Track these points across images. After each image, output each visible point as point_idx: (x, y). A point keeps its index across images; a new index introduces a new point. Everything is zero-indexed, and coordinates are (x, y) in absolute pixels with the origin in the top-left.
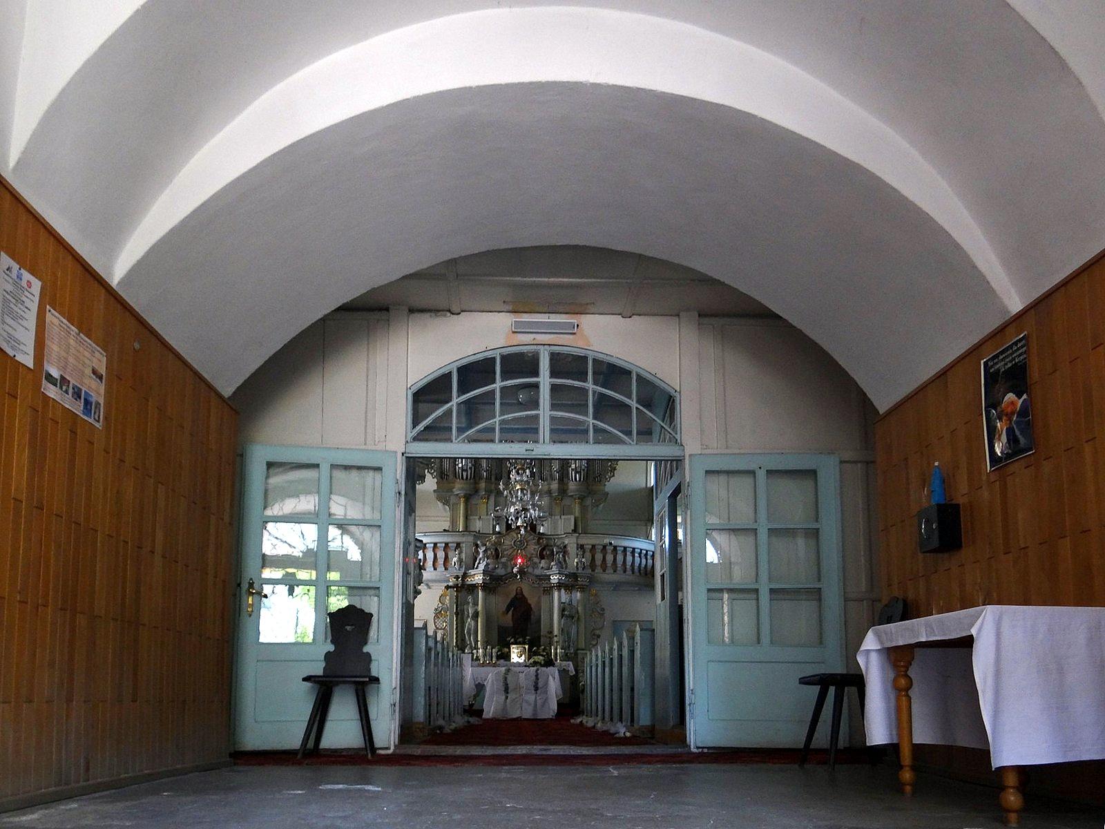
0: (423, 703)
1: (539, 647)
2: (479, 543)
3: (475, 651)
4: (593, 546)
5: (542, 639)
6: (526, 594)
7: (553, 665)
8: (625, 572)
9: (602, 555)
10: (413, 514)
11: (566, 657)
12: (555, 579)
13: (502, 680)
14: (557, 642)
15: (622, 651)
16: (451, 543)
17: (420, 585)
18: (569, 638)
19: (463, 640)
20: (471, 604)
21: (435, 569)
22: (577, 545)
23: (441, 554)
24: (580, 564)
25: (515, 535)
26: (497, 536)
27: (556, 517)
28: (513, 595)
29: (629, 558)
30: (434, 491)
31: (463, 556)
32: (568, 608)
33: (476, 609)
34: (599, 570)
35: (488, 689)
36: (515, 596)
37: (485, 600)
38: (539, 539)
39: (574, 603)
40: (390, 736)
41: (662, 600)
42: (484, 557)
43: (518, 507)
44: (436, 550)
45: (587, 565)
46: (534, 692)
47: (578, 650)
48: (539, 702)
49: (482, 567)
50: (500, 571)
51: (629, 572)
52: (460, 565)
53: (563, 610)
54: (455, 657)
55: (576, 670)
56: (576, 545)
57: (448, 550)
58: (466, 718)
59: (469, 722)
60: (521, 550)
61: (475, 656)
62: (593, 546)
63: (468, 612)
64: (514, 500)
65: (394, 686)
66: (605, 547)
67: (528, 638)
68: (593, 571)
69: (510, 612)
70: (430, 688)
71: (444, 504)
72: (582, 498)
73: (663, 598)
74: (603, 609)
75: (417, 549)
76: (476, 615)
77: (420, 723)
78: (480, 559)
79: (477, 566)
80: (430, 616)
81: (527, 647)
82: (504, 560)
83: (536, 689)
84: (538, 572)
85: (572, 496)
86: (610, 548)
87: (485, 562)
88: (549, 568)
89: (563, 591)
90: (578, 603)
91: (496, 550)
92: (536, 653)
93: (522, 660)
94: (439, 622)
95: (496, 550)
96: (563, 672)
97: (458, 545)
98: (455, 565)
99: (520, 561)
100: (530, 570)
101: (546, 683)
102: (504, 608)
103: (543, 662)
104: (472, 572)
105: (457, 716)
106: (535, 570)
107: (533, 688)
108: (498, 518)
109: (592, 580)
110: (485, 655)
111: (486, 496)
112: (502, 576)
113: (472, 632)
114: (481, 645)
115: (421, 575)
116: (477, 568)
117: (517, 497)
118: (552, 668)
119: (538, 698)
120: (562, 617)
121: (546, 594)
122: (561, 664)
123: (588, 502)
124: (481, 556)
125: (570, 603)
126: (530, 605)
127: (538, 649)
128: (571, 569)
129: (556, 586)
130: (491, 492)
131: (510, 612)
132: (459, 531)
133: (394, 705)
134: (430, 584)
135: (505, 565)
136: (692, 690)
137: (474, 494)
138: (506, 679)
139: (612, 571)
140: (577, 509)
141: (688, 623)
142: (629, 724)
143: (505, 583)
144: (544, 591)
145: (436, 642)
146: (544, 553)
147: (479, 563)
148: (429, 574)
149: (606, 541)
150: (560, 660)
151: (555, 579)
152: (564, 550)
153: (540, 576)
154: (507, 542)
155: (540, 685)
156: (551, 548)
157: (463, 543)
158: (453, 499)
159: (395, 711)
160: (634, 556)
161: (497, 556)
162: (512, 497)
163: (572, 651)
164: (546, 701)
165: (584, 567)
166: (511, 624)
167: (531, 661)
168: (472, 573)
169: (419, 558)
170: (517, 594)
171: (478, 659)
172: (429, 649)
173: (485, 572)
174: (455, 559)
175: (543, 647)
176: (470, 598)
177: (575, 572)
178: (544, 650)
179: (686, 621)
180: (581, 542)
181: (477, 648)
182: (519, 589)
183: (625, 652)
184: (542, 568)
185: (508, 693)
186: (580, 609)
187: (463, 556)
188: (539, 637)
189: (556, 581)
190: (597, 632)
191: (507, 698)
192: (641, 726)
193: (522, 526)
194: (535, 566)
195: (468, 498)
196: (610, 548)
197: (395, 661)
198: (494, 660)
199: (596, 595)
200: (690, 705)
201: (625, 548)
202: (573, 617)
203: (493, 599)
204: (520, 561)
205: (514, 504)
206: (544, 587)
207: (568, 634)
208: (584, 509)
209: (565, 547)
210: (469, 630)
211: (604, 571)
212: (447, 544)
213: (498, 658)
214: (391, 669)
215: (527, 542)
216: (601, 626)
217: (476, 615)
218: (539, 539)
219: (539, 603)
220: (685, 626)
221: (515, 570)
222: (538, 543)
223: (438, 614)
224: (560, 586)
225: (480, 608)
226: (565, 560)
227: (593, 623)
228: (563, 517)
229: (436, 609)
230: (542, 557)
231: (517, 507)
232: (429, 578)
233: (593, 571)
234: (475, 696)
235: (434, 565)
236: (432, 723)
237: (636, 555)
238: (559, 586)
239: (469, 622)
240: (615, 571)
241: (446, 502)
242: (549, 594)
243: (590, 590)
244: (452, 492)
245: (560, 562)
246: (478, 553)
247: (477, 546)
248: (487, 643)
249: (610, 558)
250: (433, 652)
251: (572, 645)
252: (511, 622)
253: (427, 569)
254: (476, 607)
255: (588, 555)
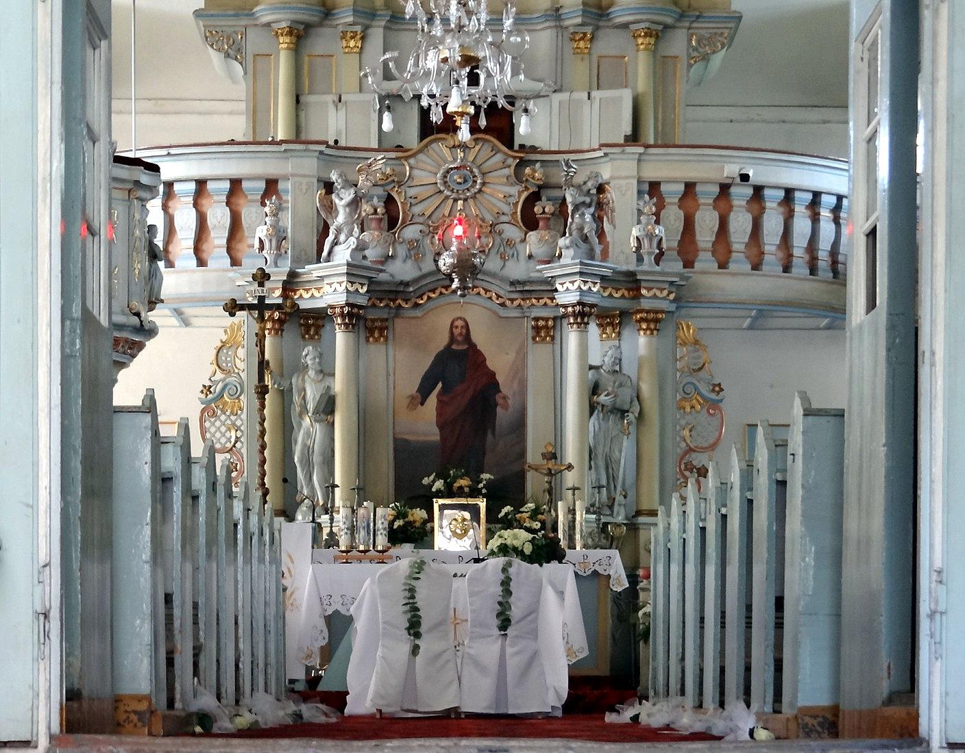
0: (147, 637)
1: (519, 504)
2: (334, 177)
3: (325, 518)
4: (690, 187)
5: (530, 476)
6: (478, 337)
7: (557, 555)
8: (787, 268)
9: (716, 215)
10: (104, 44)
11: (604, 536)
12: (568, 294)
13: (401, 597)
14: (574, 489)
15: (751, 489)
16: (249, 179)
17: (151, 310)
18: (612, 478)
19: (288, 480)
20: (311, 373)
21: (201, 263)
22: (640, 182)
23: (218, 216)
24: (646, 243)
25: (446, 152)
26: (393, 155)
27: (576, 95)
28: (442, 341)
29: (802, 225)
30: (198, 14)
31: (287, 220)
32: (608, 383)
33: (329, 388)
34: (705, 262)
35: (360, 625)
36: (448, 347)
37: (356, 355)
38: (522, 163)
39: (629, 368)
40: (34, 709)
41: (868, 312)
42: (349, 223)
43: (451, 49)
44: (204, 202)
45: (669, 249)
46: (496, 632)
47: (639, 513)
48: (513, 664)
49: (343, 254)
50: (402, 270)
51: (800, 267)
52: (279, 247)
53: (595, 389)
54: (254, 519)
55: (633, 578)
56: (635, 182)
57: (242, 201)
58: (292, 707)
59: (299, 716)
60: (465, 200)
61: (326, 531)
62: (690, 187)
63: (304, 398)
64: (438, 30)
65: (43, 558)
66: (725, 188)
67: (486, 476)
68: (688, 264)
69: (432, 400)
70: (168, 599)
71: (227, 56)
72: (658, 33)
73: (871, 304)
74: (718, 388)
75: (137, 192)
76: (327, 407)
77: (140, 699)
78: (339, 231)
79: (330, 253)
80: (192, 409)
81: (482, 504)
82: (411, 232)
83: (505, 624)
84: (517, 270)
85: (625, 26)
86: (741, 193)
87: (353, 240)
88: (552, 258)
89: (593, 329)
90: (640, 367)
91: (389, 201)
92: (508, 524)
93: (463, 545)
94: (211, 426)
95: (389, 201)
96: (591, 581)
97: (271, 186)
98: (262, 248)
99: (458, 230)
100: (493, 264)
101: (534, 610)
102: (410, 384)
103: (528, 549)
104: (313, 271)
105: (260, 693)
106: (510, 264)
107: (496, 622)
108: (390, 101)
109: (683, 295)
110: (352, 530)
111: (358, 28)
112: (407, 284)
113: (316, 458)
114: (344, 499)
115: (153, 277)
116: (328, 260)
117: (445, 21)
118: (554, 565)
119: (509, 650)
120: (591, 414)
121: (377, 340)
122: (586, 557)
123: (678, 44)
124: (341, 219)
125: (617, 370)
126: (492, 375)
127: (517, 510)
128: (621, 256)
129: (575, 315)
130: (372, 15)
131: (432, 400)
132: (274, 143)
133: (46, 616)
134: (189, 311)
135: (415, 250)
136: (939, 572)
137: (320, 25)
138: (412, 591)
139: (747, 267)
140: (642, 78)
141: (933, 365)
142: (768, 708)
143: (416, 305)
144: (537, 329)
145: (188, 461)
146: (537, 209)
147: (336, 243)
148: (184, 277)
149: (731, 170)
150: (585, 546)
151: (568, 294)
152: (598, 198)
153: (523, 283)
154: (422, 176)
155: (515, 612)
156: (556, 193)
157: (286, 178)
158: (255, 42)
159: (47, 635)
160: (815, 218)
161: (391, 219)
162: (430, 20)
163: (620, 519)
164: (533, 659)
165: (661, 254)
166: (434, 435)
167: (495, 543)
168: (316, 274)
169: (150, 221)
170: (452, 339)
171: (332, 541)
172: (163, 481)
173: (354, 272)
174: (262, 232)
175: (531, 505)
176: (309, 354)
177: (632, 267)
178: (535, 514)
179: (927, 355)
180: (652, 172)
181: (329, 510)
182: (459, 323)
183: (763, 483)
184: (530, 257)
185: (417, 635)
186: (646, 389)
187: (287, 220)
188: (521, 476)
189: (573, 298)
190: (698, 460)
191: (415, 650)
192: (801, 710)
193: (462, 114)
194: (507, 249)
195: (300, 34)
196: (741, 193)
197: (44, 482)
198: (382, 541)
199: (696, 342)
200: (931, 616)
201: (789, 192)
202: (623, 413)
203: (377, 353)
204: (458, 230)
205: (434, 43)
206: (537, 319)
207: (610, 464)
208: (662, 68)
209: (601, 189)
210: (308, 452)
211: (723, 265)
212: (236, 184)
213: (396, 537)
214: (33, 507)
215: (484, 174)
216: (711, 441)
217: (327, 407)
218: (522, 163)
219: (519, 371)
220: (924, 372)
221: (446, 261)
222: (518, 176)
223: (213, 402)
224: (583, 313)
225: (339, 385)
226: (601, 234)
227: (686, 433)
228: (595, 94)
229: (207, 389)
230: (530, 222)
231: (446, 54)
232: (185, 290)
233: (688, 264)
234: (328, 653)
235: (197, 250)
236: (178, 705)
237: (825, 214)
238: (582, 314)
239: (308, 429)
240: (756, 267)
241: (233, 50)
242: (553, 338)
243: (678, 327)
244: (251, 15)
245: (585, 239)
246: (331, 208)
247: (329, 187)
248: (362, 492)
249: (740, 223)
250: (177, 490)
251: (619, 498)
252: (437, 431)
253: (177, 264)
254: (328, 381)
255: (673, 215)
